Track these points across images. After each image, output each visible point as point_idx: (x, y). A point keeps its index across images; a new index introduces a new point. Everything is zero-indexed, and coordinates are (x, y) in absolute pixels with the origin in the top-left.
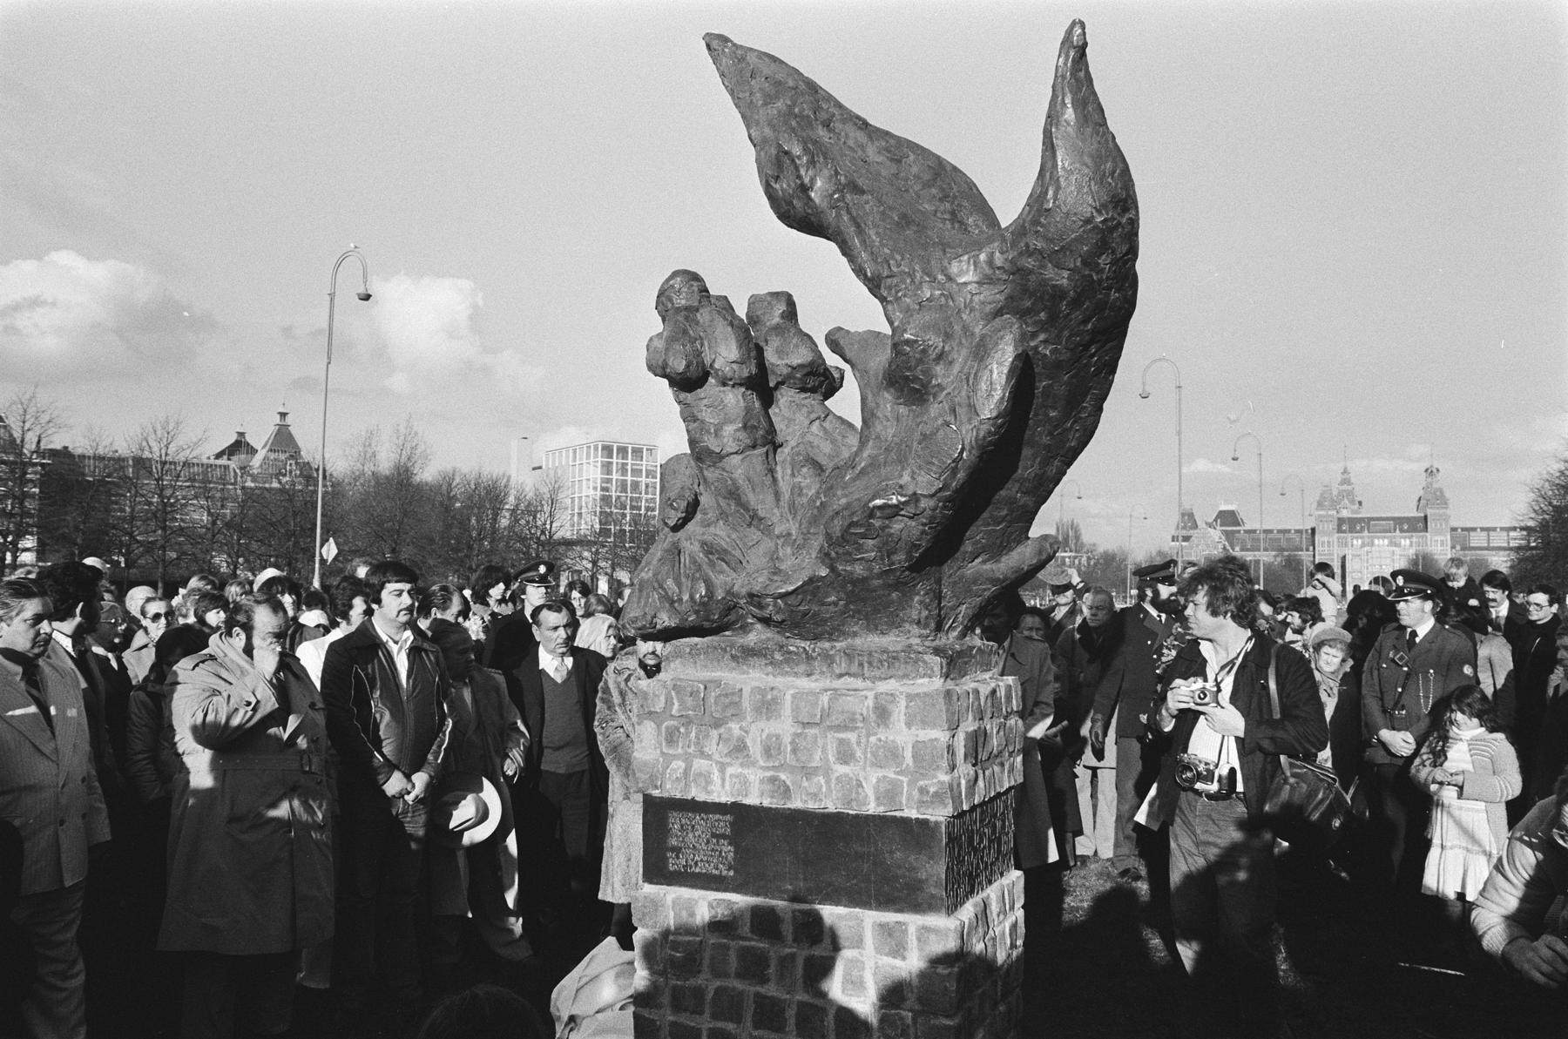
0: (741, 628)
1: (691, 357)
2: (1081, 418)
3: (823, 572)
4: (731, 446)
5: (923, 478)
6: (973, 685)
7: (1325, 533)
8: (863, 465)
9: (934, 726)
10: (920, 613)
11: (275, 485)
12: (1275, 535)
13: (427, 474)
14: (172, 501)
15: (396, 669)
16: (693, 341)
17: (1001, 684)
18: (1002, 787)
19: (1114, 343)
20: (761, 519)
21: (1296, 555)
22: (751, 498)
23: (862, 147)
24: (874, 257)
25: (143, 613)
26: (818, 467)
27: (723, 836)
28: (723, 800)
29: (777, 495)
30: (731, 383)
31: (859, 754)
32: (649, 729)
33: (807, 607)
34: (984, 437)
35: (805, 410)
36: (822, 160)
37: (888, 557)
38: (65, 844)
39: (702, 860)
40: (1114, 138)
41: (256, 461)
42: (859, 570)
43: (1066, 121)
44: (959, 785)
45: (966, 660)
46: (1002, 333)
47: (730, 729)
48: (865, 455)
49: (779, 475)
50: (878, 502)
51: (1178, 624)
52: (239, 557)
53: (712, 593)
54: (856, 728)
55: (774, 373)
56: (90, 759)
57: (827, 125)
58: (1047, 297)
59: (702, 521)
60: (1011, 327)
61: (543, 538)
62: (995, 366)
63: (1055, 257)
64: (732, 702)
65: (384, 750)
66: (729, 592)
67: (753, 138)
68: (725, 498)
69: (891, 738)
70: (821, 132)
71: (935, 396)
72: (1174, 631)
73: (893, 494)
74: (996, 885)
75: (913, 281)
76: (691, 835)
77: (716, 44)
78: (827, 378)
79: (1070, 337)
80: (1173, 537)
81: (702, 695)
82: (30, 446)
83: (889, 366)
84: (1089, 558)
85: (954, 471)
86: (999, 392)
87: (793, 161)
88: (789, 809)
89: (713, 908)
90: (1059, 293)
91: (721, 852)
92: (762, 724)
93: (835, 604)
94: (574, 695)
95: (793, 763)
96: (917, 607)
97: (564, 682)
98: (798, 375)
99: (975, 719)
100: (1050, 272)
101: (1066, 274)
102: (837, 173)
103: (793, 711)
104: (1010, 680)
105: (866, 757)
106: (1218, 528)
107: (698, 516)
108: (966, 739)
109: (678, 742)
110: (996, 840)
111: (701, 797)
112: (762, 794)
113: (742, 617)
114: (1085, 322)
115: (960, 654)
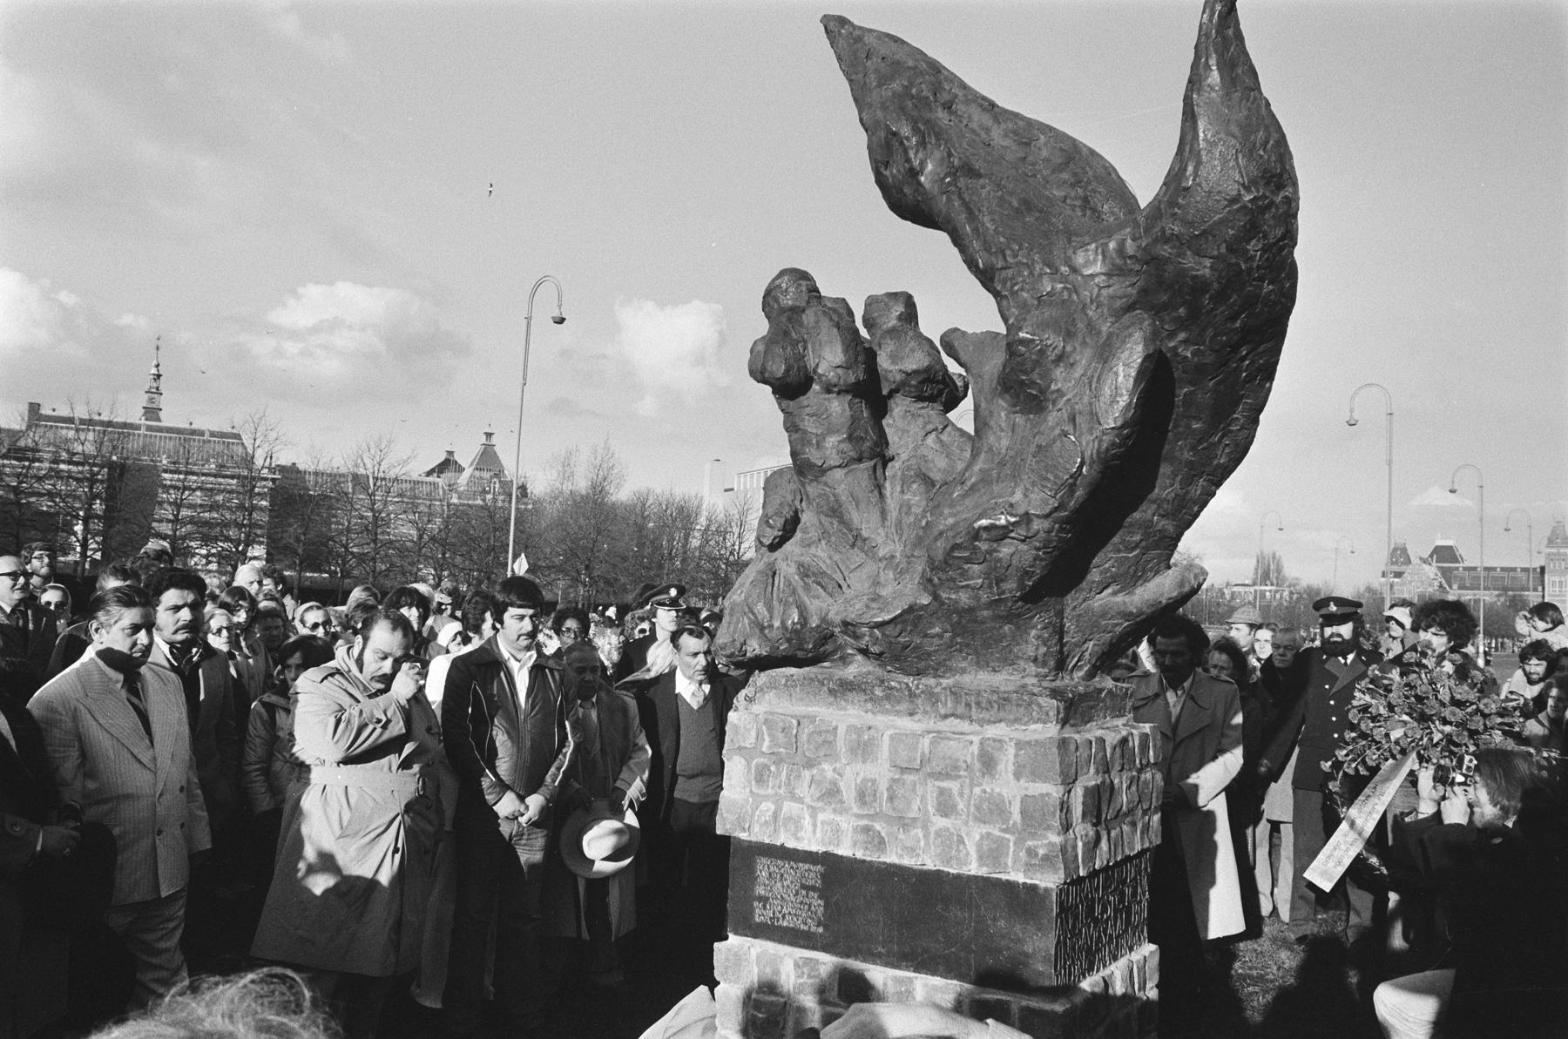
0: (841, 658)
1: (792, 361)
2: (1232, 431)
3: (925, 600)
4: (834, 460)
5: (1036, 496)
6: (1099, 733)
7: (1554, 572)
8: (973, 480)
9: (1045, 780)
10: (1037, 649)
11: (479, 502)
12: (1498, 573)
13: (622, 494)
14: (383, 515)
15: (515, 688)
16: (795, 343)
17: (1134, 732)
18: (1133, 849)
19: (1269, 345)
20: (865, 540)
21: (1521, 596)
22: (855, 517)
23: (988, 130)
24: (987, 248)
25: (303, 622)
26: (929, 482)
27: (813, 888)
28: (814, 848)
29: (883, 514)
30: (836, 389)
31: (961, 806)
32: (739, 766)
33: (907, 639)
34: (1107, 450)
35: (920, 421)
36: (933, 141)
37: (997, 584)
38: (161, 851)
39: (790, 913)
40: (1268, 104)
41: (464, 478)
42: (964, 598)
43: (1209, 86)
44: (1075, 847)
45: (1092, 703)
46: (1130, 330)
47: (823, 770)
48: (976, 468)
49: (887, 492)
50: (984, 522)
51: (1375, 666)
52: (442, 570)
53: (805, 619)
54: (960, 777)
55: (887, 379)
56: (191, 767)
57: (948, 106)
58: (1186, 290)
59: (802, 540)
60: (1141, 323)
61: (732, 558)
62: (1121, 368)
63: (1194, 243)
64: (825, 741)
65: (498, 770)
66: (824, 620)
67: (865, 121)
68: (827, 515)
69: (997, 790)
70: (941, 115)
71: (1054, 402)
72: (1369, 673)
73: (1002, 513)
74: (1122, 962)
75: (1031, 273)
76: (779, 884)
77: (835, 27)
78: (947, 385)
79: (1215, 335)
80: (1384, 573)
81: (795, 732)
82: (259, 462)
83: (1004, 369)
84: (1291, 593)
85: (1072, 488)
86: (1126, 398)
87: (902, 143)
88: (885, 863)
89: (799, 967)
90: (1200, 286)
91: (810, 906)
92: (859, 766)
93: (940, 636)
94: (710, 721)
95: (891, 813)
96: (1033, 641)
97: (700, 708)
98: (913, 383)
99: (1097, 772)
100: (1189, 261)
101: (1208, 262)
102: (950, 155)
103: (891, 753)
104: (1147, 728)
105: (968, 812)
106: (1434, 564)
107: (798, 535)
108: (1085, 796)
109: (768, 781)
110: (1124, 910)
111: (791, 844)
112: (855, 844)
113: (841, 647)
114: (1233, 318)
115: (1084, 697)
